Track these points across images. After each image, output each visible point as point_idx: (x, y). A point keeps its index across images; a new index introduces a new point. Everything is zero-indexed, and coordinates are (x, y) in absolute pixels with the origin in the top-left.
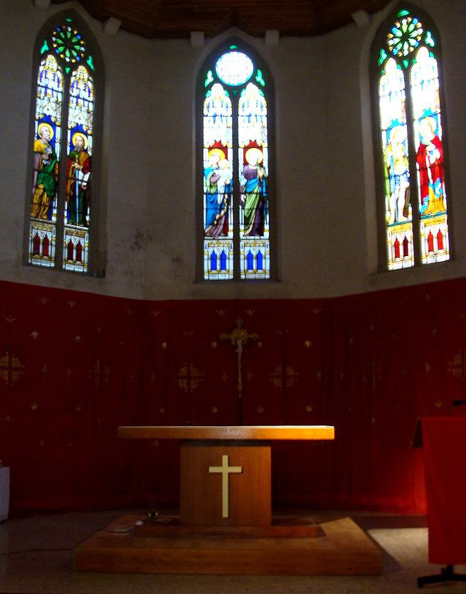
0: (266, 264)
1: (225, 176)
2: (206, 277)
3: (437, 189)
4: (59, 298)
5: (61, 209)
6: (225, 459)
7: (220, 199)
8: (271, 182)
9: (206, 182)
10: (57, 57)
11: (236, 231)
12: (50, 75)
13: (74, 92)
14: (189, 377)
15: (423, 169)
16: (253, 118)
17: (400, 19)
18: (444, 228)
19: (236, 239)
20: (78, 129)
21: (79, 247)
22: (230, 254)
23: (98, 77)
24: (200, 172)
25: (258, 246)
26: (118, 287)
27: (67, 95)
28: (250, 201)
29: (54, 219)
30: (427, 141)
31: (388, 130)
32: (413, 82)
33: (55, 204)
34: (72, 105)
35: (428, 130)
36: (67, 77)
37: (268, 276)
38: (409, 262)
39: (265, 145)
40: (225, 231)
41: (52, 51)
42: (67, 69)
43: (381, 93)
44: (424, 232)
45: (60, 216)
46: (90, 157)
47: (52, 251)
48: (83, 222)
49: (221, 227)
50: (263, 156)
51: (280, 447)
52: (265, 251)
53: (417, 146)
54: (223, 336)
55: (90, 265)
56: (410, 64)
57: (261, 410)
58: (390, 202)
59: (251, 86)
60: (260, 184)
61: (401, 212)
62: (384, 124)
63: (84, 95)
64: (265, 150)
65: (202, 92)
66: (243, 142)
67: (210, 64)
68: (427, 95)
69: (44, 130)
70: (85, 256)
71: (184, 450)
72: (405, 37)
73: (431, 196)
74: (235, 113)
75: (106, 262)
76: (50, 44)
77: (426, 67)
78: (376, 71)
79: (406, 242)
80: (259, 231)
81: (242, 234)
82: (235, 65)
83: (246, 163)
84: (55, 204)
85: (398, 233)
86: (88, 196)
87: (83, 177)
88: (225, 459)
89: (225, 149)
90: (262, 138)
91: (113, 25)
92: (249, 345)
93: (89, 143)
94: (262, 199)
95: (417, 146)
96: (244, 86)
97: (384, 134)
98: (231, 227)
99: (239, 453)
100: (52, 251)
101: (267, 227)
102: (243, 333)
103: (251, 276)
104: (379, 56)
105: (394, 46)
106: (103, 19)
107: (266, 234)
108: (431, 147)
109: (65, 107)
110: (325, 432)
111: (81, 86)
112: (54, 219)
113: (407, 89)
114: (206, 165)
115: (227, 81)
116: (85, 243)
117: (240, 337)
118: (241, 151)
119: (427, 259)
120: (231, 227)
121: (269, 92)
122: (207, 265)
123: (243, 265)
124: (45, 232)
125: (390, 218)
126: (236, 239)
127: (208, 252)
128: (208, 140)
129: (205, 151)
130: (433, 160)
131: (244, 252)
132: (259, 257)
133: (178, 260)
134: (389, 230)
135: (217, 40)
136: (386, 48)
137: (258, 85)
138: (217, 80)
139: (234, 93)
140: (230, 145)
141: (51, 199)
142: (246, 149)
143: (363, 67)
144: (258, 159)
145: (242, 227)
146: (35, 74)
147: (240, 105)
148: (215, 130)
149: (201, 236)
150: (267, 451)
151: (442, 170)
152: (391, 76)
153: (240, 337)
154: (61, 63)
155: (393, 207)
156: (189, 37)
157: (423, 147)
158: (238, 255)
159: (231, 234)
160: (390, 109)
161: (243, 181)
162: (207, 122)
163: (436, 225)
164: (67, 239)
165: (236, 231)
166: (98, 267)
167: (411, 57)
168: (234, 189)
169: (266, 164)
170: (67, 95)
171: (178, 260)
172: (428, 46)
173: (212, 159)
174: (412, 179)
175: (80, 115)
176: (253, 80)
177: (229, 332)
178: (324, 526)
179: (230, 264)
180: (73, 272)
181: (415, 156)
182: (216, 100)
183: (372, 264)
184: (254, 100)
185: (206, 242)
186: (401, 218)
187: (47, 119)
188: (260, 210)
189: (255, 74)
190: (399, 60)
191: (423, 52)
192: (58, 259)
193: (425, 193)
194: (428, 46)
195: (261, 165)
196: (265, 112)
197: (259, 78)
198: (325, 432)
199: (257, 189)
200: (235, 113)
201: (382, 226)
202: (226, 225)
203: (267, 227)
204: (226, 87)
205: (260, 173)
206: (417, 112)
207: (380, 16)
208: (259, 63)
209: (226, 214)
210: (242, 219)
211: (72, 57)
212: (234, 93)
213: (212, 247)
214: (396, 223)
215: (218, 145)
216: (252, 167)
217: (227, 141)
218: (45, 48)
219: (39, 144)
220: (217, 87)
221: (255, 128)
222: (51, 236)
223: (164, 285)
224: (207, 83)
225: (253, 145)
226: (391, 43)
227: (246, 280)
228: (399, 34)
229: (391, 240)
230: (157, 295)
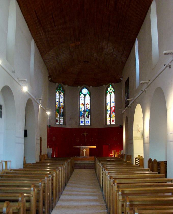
0: (89, 123)
1: (83, 109)
2: (80, 124)
3: (114, 113)
4: (60, 128)
5: (59, 114)
6: (84, 150)
7: (82, 112)
8: (90, 110)
9: (80, 110)
10: (58, 92)
11: (85, 117)
12: (57, 94)
13: (61, 97)
14: (78, 140)
15: (112, 110)
16: (88, 100)
17: (110, 86)
18: (114, 119)
19: (85, 119)
20: (62, 102)
21: (62, 121)
22: (84, 121)
23: (64, 94)
24: (80, 108)
25: (88, 120)
26: (68, 126)
27: (60, 97)
28: (87, 113)
29: (59, 117)
30: (113, 106)
31: (108, 103)
32: (111, 97)
33: (59, 114)
34: (61, 99)
35: (113, 104)
36: (60, 94)
37: (89, 124)
38: (110, 124)
39: (89, 104)
40: (83, 118)
41: (58, 91)
42: (60, 93)
43: (107, 97)
44: (112, 119)
45: (59, 116)
46: (63, 107)
47: (58, 121)
48: (62, 117)
49: (83, 117)
50: (89, 106)
51: (90, 148)
52: (89, 121)
53: (111, 107)
54: (83, 134)
55: (63, 123)
56: (111, 94)
57: (82, 144)
58: (107, 114)
59: (87, 94)
60: (89, 110)
61: (109, 116)
62: (107, 102)
63: (62, 97)
64: (89, 105)
65: (80, 95)
66: (86, 103)
67: (81, 90)
68: (113, 100)
69: (57, 103)
70: (63, 122)
71: (28, 162)
72: (111, 89)
73: (113, 114)
74: (85, 99)
75: (66, 122)
76: (58, 90)
77: (113, 95)
78: (106, 94)
79: (109, 121)
80: (88, 117)
81: (86, 118)
82: (85, 91)
83: (86, 107)
84: (59, 114)
85: (108, 119)
86: (63, 113)
87: (62, 110)
88: (84, 150)
89: (83, 105)
90: (89, 103)
91: (66, 86)
92: (87, 135)
93: (63, 104)
94: (89, 113)
95: (111, 107)
96: (86, 94)
97: (107, 104)
98: (84, 117)
99: (86, 149)
100: (58, 121)
101: (89, 117)
102: (86, 133)
103: (87, 124)
104: (107, 92)
105: (109, 90)
106: (65, 85)
107: (89, 118)
108: (113, 107)
109: (60, 99)
110: (95, 147)
111: (62, 95)
112: (59, 117)
113: (110, 97)
114: (80, 107)
115: (84, 93)
116: (63, 120)
117: (85, 134)
118: (86, 105)
119: (112, 123)
120: (84, 117)
121: (90, 95)
122: (80, 123)
123: (86, 123)
124: (57, 119)
125: (107, 117)
126: (85, 119)
127: (80, 121)
128: (81, 103)
129: (80, 105)
130: (113, 109)
131: (86, 121)
132: (88, 122)
133: (76, 122)
134: (107, 119)
135: (82, 87)
136: (108, 90)
137: (89, 94)
138: (82, 93)
139: (85, 95)
140: (84, 104)
141: (58, 114)
142: (86, 105)
143: (104, 98)
144: (88, 106)
145: (86, 117)
146: (56, 95)
147: (86, 97)
148: (82, 101)
149: (80, 118)
150: (89, 149)
151: (114, 111)
152: (108, 95)
153: (85, 134)
154: (59, 92)
155: (108, 115)
156: (78, 86)
157: (112, 107)
158: (85, 121)
159: (84, 118)
160: (108, 101)
161: (86, 110)
162: (81, 100)
163: (113, 119)
164: (60, 119)
165: (85, 117)
166: (65, 123)
167: (111, 93)
168: (85, 111)
169: (89, 107)
170: (60, 97)
171: (76, 122)
172: (113, 92)
173: (81, 106)
174: (110, 111)
175: (62, 100)
176: (88, 93)
177: (84, 133)
178: (137, 87)
179: (84, 123)
180: (61, 124)
181: (111, 108)
182: (82, 96)
183: (105, 124)
184: (88, 96)
185: (80, 119)
186: (109, 117)
187: (57, 102)
188: (89, 114)
189: (88, 92)
190: (110, 93)
191: (113, 92)
192: (59, 123)
193: (112, 114)
194: (113, 92)
195: (89, 107)
196: (89, 99)
197: (89, 93)
198: (95, 147)
199: (88, 111)
200: (85, 99)
201: (106, 118)
202: (83, 116)
203: (89, 117)
204: (83, 94)
205: (89, 108)
206: (112, 102)
207: (107, 85)
208: (89, 90)
209: (83, 115)
210: (86, 116)
211: (60, 91)
212: (85, 95)
213: (81, 120)
214: (108, 118)
215: (82, 104)
216: (87, 107)
217: (84, 103)
218: (57, 90)
219: (57, 106)
220: (82, 94)
221: (88, 101)
222: (58, 119)
223: (75, 126)
224: (81, 94)
225: (88, 104)
226: (109, 90)
227: (86, 125)
228: (109, 90)
229: (107, 120)
230: (73, 127)
